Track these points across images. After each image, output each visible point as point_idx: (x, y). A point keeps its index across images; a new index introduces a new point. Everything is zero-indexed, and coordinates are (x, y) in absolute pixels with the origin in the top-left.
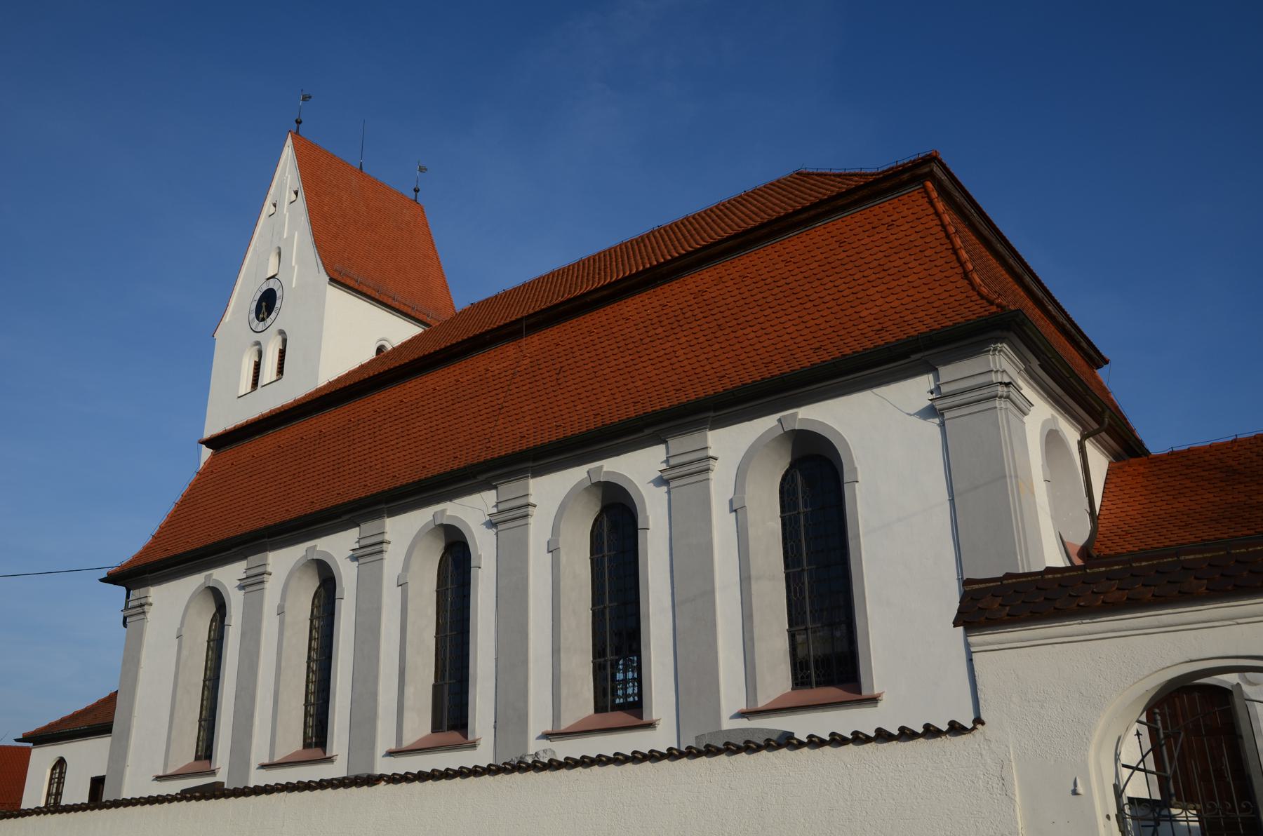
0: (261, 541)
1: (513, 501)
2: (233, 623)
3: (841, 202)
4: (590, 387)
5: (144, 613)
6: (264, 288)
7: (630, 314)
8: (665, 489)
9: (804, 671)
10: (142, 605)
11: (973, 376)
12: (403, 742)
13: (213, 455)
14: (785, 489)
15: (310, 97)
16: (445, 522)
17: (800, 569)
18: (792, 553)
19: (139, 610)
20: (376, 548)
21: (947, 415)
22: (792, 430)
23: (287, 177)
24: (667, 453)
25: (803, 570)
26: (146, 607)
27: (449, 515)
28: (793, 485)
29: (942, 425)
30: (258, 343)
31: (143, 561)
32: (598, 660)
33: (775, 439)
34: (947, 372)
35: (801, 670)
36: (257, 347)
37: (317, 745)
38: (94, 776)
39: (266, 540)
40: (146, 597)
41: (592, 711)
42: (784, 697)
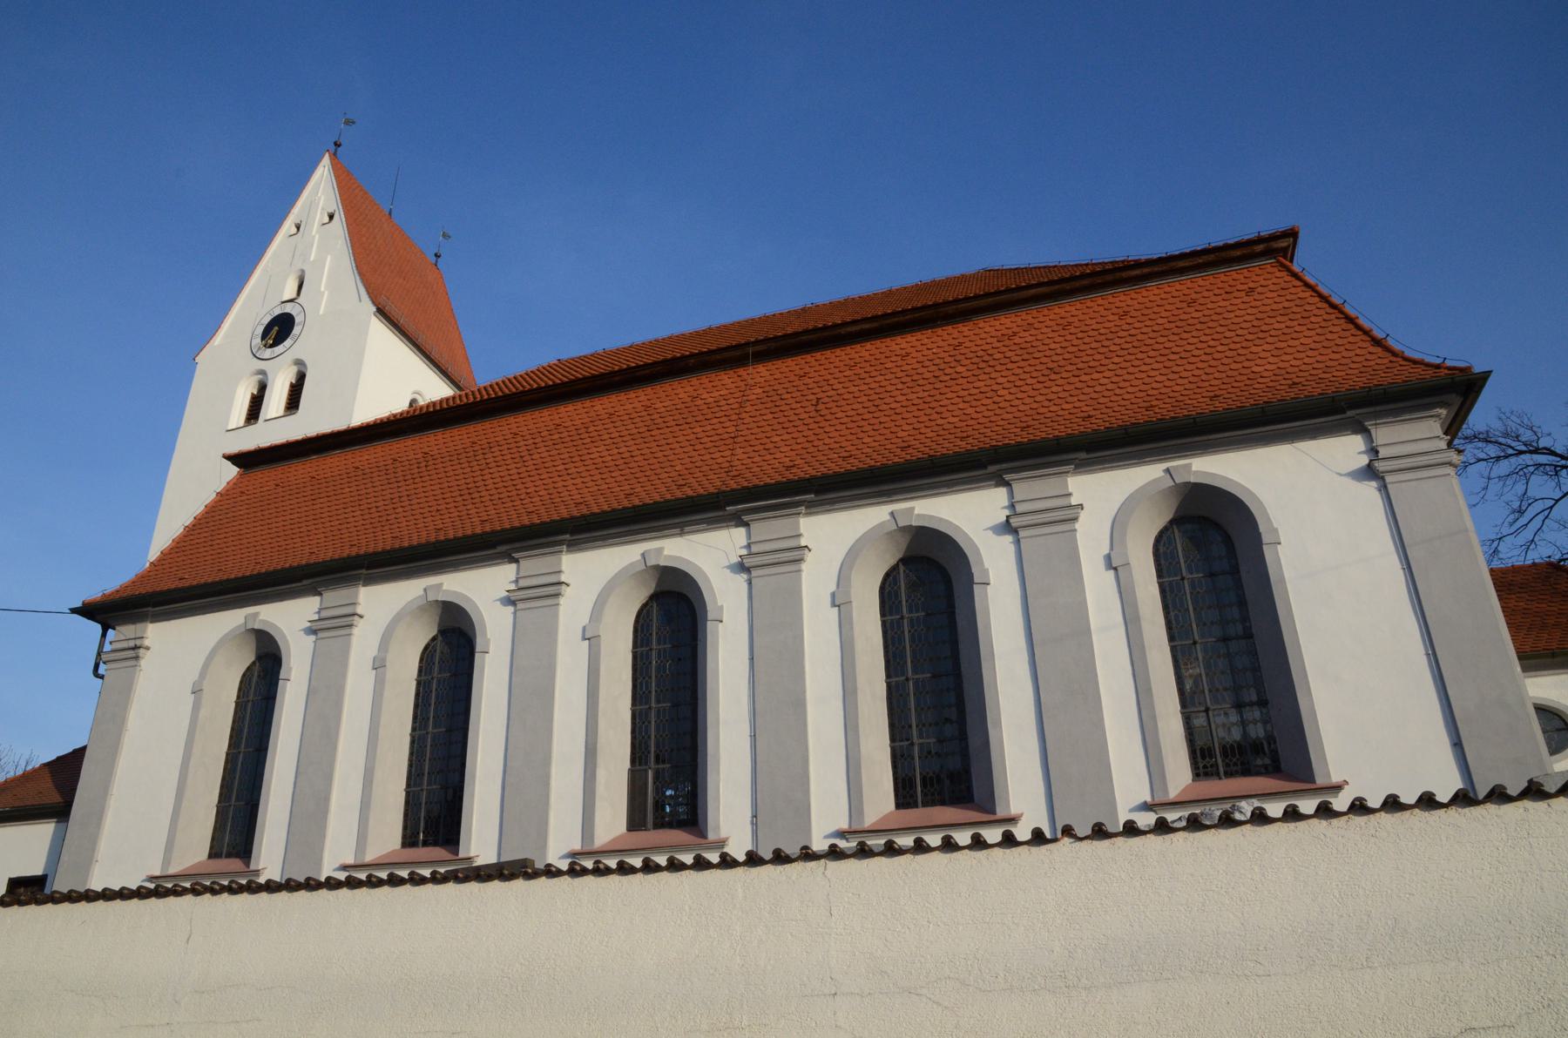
0: (140, 610)
1: (792, 539)
2: (293, 676)
3: (1181, 264)
4: (290, 532)
5: (137, 658)
6: (278, 312)
7: (399, 455)
8: (511, 609)
10: (136, 648)
11: (1416, 440)
12: (596, 841)
13: (241, 475)
14: (1161, 551)
15: (353, 123)
16: (256, 627)
17: (647, 706)
18: (641, 689)
19: (131, 653)
20: (551, 590)
21: (1022, 533)
23: (320, 198)
24: (518, 573)
25: (907, 679)
26: (142, 651)
27: (918, 515)
29: (1018, 542)
30: (263, 372)
31: (129, 593)
32: (223, 804)
35: (1203, 757)
36: (260, 376)
37: (237, 856)
38: (14, 875)
39: (150, 609)
40: (142, 638)
41: (400, 846)
42: (886, 818)
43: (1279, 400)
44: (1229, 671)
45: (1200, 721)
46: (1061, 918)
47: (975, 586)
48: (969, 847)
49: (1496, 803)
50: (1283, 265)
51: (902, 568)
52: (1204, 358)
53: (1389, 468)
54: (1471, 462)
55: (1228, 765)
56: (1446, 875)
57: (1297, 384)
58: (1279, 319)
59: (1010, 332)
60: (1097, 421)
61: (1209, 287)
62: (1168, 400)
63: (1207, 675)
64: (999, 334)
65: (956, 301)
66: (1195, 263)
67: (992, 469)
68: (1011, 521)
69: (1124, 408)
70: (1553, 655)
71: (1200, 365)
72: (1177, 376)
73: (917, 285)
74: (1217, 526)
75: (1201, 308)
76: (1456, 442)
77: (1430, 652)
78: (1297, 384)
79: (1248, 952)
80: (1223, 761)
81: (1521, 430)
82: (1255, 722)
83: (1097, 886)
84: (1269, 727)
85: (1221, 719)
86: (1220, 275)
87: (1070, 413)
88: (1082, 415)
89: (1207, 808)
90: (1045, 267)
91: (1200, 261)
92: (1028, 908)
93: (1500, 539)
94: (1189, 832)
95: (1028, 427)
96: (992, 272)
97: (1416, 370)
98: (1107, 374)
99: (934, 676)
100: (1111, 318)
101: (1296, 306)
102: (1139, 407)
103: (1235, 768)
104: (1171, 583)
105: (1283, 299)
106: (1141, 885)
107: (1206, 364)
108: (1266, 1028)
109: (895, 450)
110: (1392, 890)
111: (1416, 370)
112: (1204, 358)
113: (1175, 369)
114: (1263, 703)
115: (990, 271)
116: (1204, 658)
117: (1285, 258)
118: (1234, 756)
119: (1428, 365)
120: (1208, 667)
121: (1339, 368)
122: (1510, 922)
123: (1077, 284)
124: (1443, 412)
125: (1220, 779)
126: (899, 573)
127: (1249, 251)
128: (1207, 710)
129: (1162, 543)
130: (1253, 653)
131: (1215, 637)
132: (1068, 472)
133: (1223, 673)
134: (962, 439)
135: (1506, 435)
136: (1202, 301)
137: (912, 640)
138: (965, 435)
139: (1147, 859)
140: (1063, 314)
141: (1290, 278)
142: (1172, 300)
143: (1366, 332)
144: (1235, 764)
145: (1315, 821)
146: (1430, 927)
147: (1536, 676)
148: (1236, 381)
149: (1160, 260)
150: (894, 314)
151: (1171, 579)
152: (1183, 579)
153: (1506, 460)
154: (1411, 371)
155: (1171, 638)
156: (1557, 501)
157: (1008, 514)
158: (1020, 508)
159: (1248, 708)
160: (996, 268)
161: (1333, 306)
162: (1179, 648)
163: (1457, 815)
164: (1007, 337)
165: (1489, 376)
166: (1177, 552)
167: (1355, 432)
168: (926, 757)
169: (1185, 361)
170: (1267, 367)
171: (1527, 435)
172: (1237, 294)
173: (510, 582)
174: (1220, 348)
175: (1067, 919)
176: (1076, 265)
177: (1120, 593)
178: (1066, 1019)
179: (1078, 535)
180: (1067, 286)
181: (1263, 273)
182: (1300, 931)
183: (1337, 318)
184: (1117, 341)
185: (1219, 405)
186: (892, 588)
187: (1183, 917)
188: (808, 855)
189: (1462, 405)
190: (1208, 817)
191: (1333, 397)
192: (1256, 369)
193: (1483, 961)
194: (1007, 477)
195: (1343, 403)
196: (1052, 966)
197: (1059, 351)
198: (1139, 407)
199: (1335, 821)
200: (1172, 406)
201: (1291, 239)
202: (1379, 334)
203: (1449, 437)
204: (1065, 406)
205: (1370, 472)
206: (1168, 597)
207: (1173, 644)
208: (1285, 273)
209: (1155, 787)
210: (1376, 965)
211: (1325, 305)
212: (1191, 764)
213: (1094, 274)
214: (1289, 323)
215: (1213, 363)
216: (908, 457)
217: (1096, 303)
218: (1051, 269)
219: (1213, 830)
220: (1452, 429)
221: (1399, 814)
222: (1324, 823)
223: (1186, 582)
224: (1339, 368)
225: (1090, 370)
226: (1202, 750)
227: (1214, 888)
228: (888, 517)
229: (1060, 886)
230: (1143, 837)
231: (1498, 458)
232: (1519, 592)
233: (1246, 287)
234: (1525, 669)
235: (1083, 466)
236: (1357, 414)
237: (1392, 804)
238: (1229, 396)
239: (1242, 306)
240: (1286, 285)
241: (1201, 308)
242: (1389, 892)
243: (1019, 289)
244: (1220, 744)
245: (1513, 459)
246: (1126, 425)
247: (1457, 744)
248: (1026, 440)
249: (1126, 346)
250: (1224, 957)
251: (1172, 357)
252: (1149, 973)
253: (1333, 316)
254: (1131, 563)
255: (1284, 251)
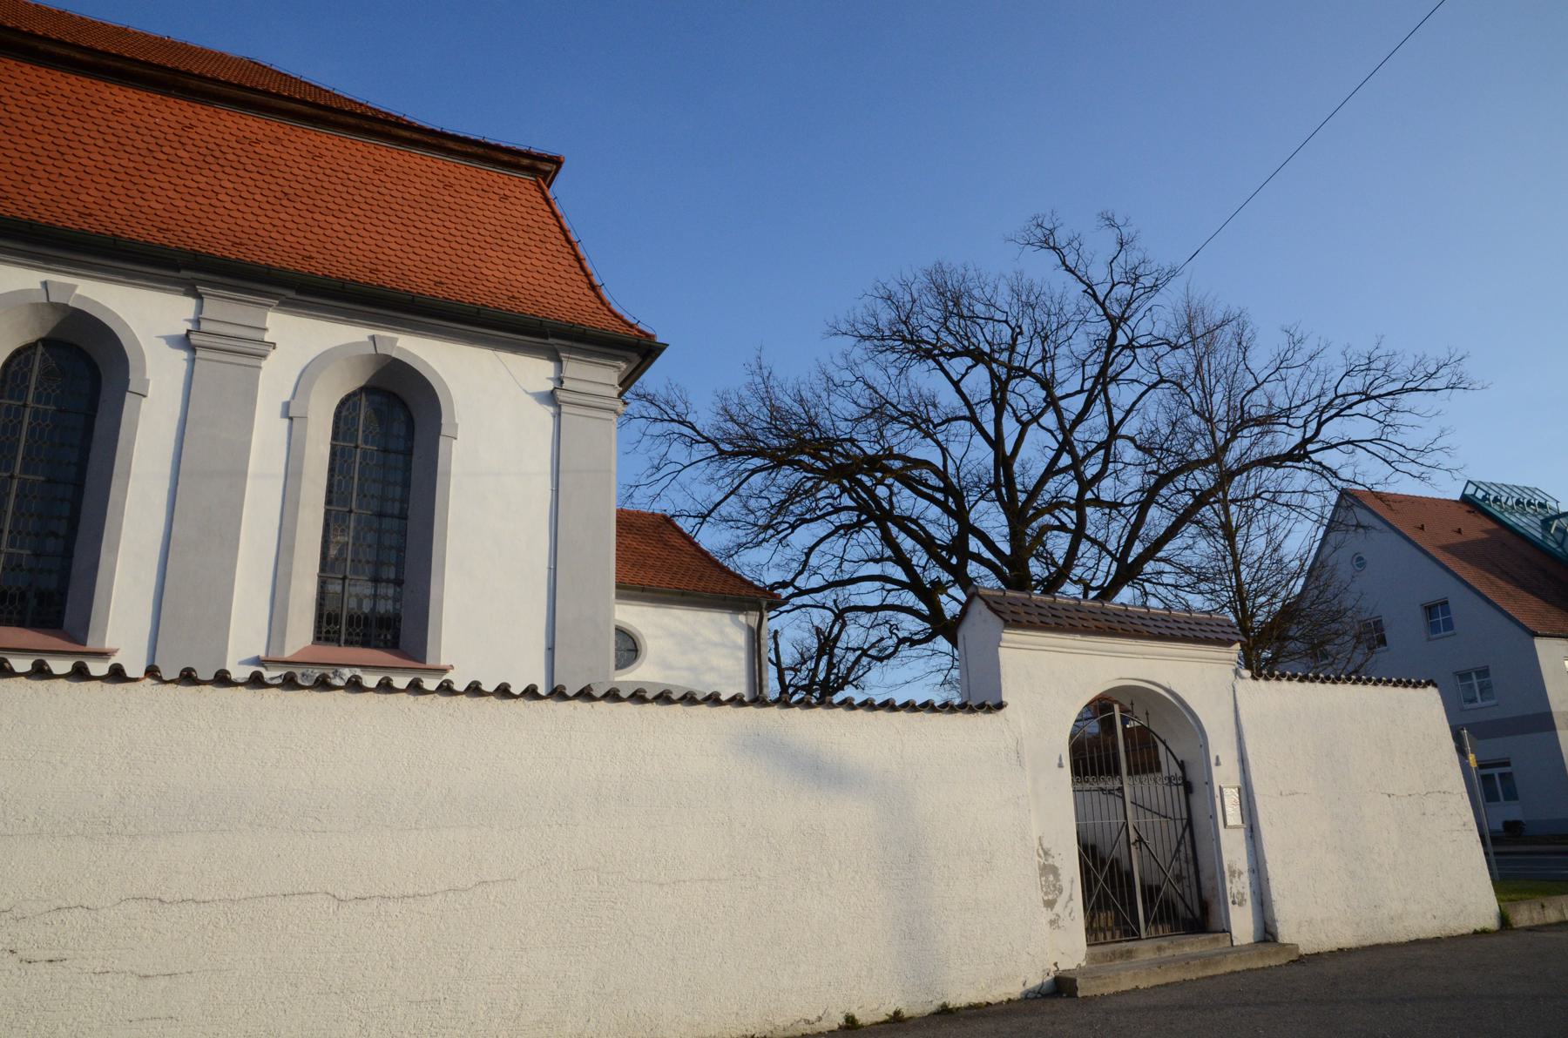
1: (229, 326)
3: (451, 145)
9: (332, 625)
14: (344, 413)
21: (200, 353)
22: (387, 355)
28: (354, 414)
29: (192, 361)
33: (362, 356)
34: (213, 307)
35: (329, 623)
43: (495, 307)
44: (376, 546)
45: (335, 587)
46: (121, 761)
47: (128, 393)
48: (27, 675)
49: (554, 700)
50: (539, 186)
51: (40, 349)
52: (442, 242)
53: (568, 400)
54: (636, 416)
55: (350, 634)
56: (500, 756)
57: (516, 298)
58: (521, 233)
59: (253, 137)
60: (316, 265)
61: (469, 178)
62: (394, 270)
63: (354, 544)
64: (241, 134)
65: (200, 77)
66: (464, 149)
67: (185, 274)
68: (191, 337)
69: (349, 262)
70: (643, 590)
71: (436, 248)
72: (410, 250)
73: (162, 39)
74: (404, 405)
75: (455, 194)
76: (627, 394)
77: (552, 567)
78: (516, 298)
79: (310, 809)
80: (347, 630)
81: (678, 403)
82: (386, 598)
83: (170, 732)
84: (398, 607)
85: (357, 590)
86: (504, 176)
87: (291, 247)
88: (436, 279)
89: (310, 670)
90: (316, 87)
91: (469, 150)
92: (83, 748)
93: (637, 486)
94: (282, 690)
95: (241, 244)
96: (257, 66)
97: (613, 322)
98: (343, 222)
99: (48, 481)
100: (366, 167)
101: (539, 228)
102: (364, 267)
103: (357, 638)
104: (343, 448)
105: (529, 217)
106: (219, 735)
107: (442, 250)
108: (309, 880)
109: (72, 213)
110: (453, 764)
111: (613, 322)
112: (442, 242)
113: (412, 243)
114: (398, 582)
115: (255, 63)
116: (355, 528)
117: (544, 181)
118: (358, 626)
119: (625, 322)
120: (356, 538)
121: (556, 297)
122: (537, 797)
123: (342, 119)
124: (623, 365)
125: (340, 646)
126: (35, 354)
127: (516, 161)
128: (344, 579)
129: (347, 406)
130: (403, 533)
131: (371, 510)
132: (270, 306)
133: (370, 546)
134: (160, 230)
135: (667, 403)
136: (458, 188)
137: (31, 433)
138: (165, 226)
139: (232, 711)
140: (318, 143)
141: (541, 201)
142: (430, 176)
143: (587, 275)
144: (358, 634)
145: (404, 695)
146: (476, 798)
147: (627, 604)
148: (464, 276)
149: (432, 132)
150: (119, 57)
151: (345, 444)
152: (356, 447)
153: (661, 424)
154: (610, 321)
155: (329, 502)
156: (685, 467)
157: (190, 328)
158: (205, 326)
159: (384, 584)
160: (264, 64)
161: (568, 241)
162: (333, 513)
163: (523, 706)
164: (248, 141)
165: (665, 348)
166: (359, 419)
167: (550, 359)
168: (13, 570)
169: (423, 239)
170: (494, 273)
171: (680, 408)
172: (492, 195)
173: (186, 320)
174: (460, 239)
175: (128, 763)
176: (350, 100)
177: (289, 444)
178: (98, 867)
179: (261, 373)
180: (332, 117)
181: (520, 186)
182: (364, 793)
183: (568, 253)
184: (364, 193)
185: (441, 293)
186: (21, 369)
187: (255, 771)
188: (223, 679)
189: (638, 366)
190: (309, 678)
191: (541, 321)
192: (485, 271)
193: (509, 828)
194: (201, 289)
195: (548, 330)
196: (97, 811)
197: (300, 179)
198: (364, 267)
199: (421, 698)
200: (397, 277)
201: (555, 167)
202: (597, 281)
203: (621, 389)
204: (288, 238)
205: (551, 398)
206: (338, 461)
207: (328, 507)
208: (540, 195)
209: (271, 643)
210: (423, 827)
211: (562, 237)
212: (315, 627)
213: (363, 116)
214: (527, 241)
215: (448, 250)
216: (86, 227)
217: (355, 147)
218: (323, 93)
219: (307, 691)
220: (626, 382)
221: (478, 699)
222: (412, 698)
223: (358, 450)
224: (556, 297)
225: (326, 212)
226: (329, 615)
227: (292, 746)
228: (39, 286)
229: (129, 728)
230: (234, 688)
231: (656, 420)
232: (636, 534)
233: (501, 192)
234: (618, 596)
235: (287, 305)
236: (557, 344)
237: (503, 691)
238: (453, 287)
239: (492, 208)
240: (536, 206)
241: (455, 194)
242: (451, 765)
243: (278, 96)
244: (348, 613)
245: (666, 424)
246: (345, 280)
247: (551, 649)
248: (234, 257)
249: (371, 201)
250: (286, 812)
251: (412, 230)
252: (205, 824)
253: (566, 250)
254: (309, 416)
255: (545, 174)
